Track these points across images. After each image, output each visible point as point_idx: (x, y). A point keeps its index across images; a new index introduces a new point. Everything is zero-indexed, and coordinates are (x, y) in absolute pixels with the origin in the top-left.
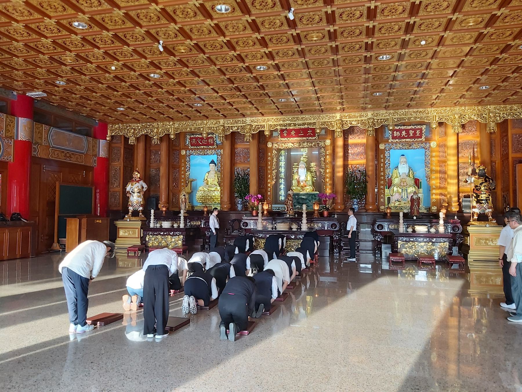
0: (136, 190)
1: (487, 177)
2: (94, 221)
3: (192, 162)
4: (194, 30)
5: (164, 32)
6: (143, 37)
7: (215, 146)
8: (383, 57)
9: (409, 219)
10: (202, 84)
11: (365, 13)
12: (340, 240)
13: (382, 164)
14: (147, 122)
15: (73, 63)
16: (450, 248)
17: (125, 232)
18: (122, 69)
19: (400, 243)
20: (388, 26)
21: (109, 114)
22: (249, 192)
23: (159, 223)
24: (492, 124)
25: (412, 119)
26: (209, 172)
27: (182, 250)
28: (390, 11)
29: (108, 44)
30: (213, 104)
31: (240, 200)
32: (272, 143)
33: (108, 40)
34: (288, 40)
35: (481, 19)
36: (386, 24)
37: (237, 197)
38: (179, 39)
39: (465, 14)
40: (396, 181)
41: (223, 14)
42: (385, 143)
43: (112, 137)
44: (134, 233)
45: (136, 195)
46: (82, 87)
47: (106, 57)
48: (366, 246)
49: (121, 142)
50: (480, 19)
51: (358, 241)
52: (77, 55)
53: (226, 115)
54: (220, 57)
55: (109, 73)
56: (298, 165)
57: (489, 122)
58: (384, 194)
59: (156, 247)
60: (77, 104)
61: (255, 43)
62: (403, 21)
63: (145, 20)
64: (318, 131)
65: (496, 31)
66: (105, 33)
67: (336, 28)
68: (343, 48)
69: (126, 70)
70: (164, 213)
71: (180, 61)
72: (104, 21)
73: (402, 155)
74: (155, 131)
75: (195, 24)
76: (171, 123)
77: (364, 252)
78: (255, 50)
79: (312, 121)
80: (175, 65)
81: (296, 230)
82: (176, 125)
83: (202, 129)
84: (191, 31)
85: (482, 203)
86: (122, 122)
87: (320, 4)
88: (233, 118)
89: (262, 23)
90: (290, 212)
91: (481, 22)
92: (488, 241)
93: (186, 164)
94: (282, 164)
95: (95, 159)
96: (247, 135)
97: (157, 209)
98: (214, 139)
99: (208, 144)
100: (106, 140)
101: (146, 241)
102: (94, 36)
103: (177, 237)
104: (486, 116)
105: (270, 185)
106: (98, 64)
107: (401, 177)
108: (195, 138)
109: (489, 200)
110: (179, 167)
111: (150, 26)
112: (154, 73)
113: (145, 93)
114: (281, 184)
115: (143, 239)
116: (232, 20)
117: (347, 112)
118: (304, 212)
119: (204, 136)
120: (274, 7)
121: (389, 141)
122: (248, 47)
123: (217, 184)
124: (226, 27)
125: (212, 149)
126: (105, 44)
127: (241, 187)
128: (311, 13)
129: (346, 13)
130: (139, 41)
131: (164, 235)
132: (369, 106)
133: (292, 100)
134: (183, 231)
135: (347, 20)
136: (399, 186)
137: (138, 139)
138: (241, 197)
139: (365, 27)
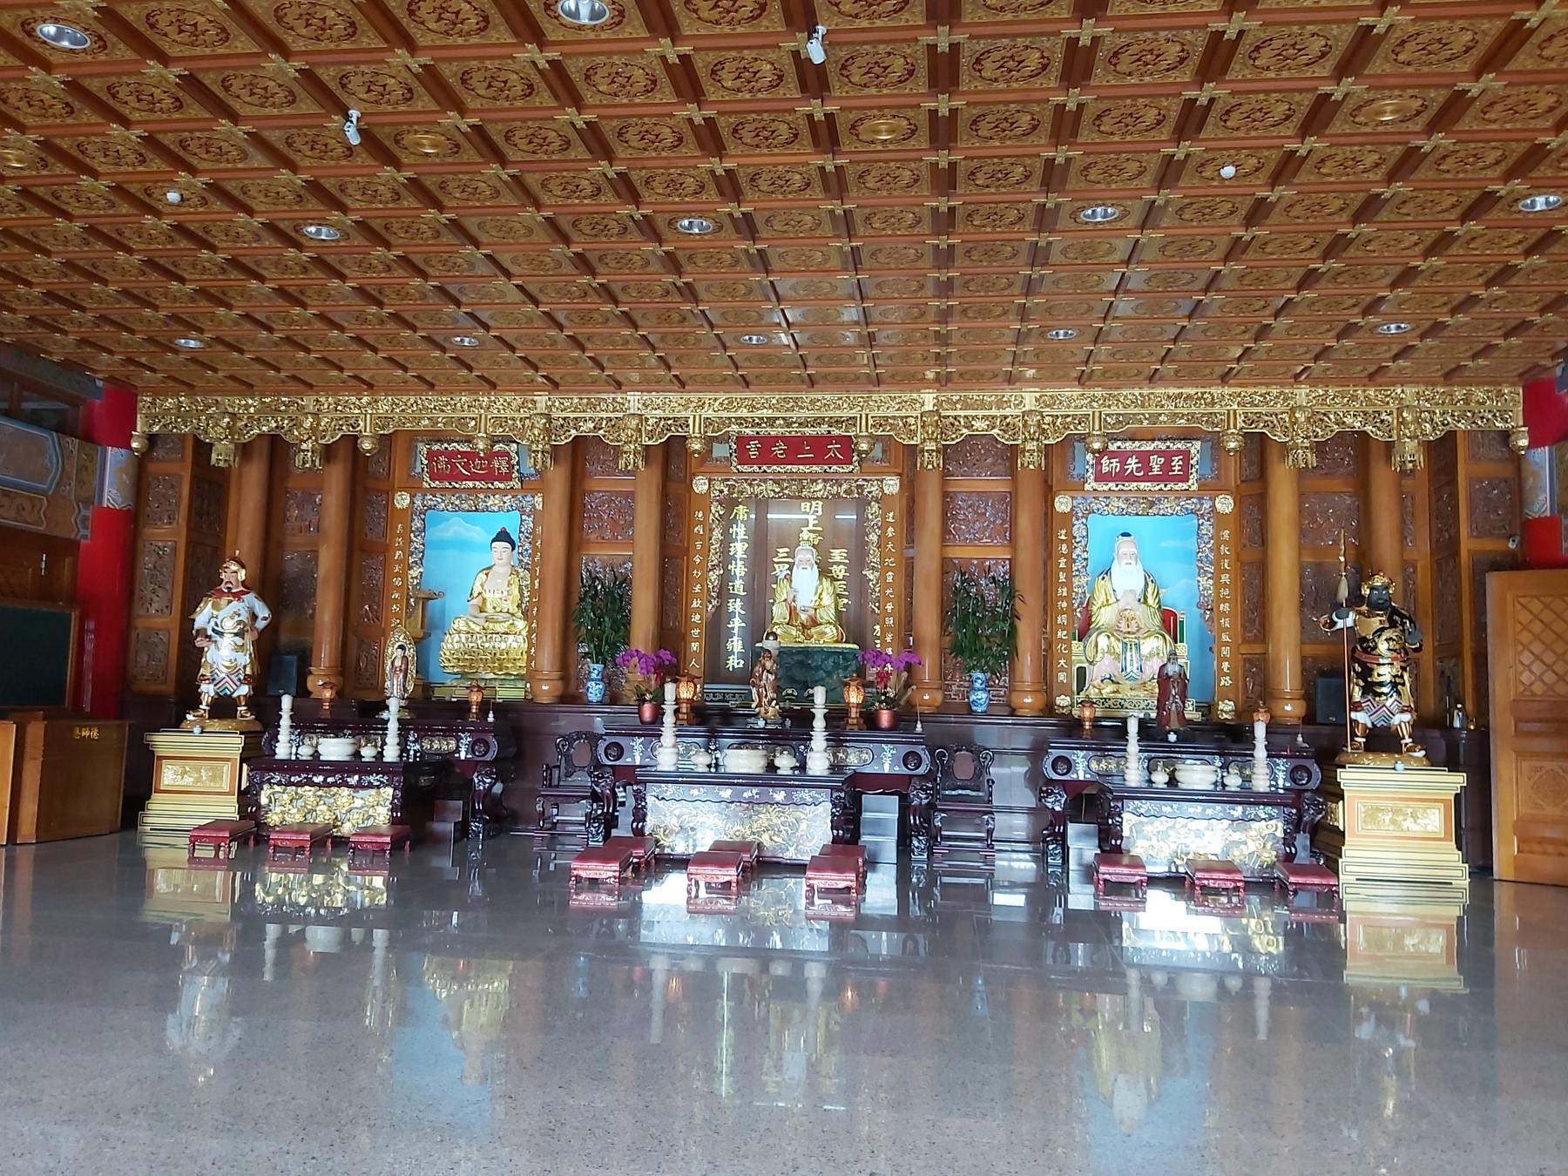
0: (229, 625)
1: (1395, 611)
2: (72, 731)
3: (433, 533)
4: (476, 80)
5: (367, 78)
6: (291, 93)
7: (516, 484)
8: (1094, 211)
9: (1154, 741)
10: (434, 299)
11: (1059, 56)
12: (932, 807)
13: (1063, 561)
14: (279, 393)
15: (26, 173)
16: (1288, 840)
17: (184, 773)
18: (205, 202)
19: (1128, 821)
20: (1123, 110)
21: (143, 360)
22: (626, 640)
23: (307, 741)
24: (1411, 446)
25: (1161, 419)
26: (490, 568)
27: (388, 840)
28: (1139, 60)
29: (161, 110)
30: (517, 340)
31: (596, 666)
32: (710, 481)
33: (163, 96)
34: (796, 136)
35: (1420, 102)
36: (989, 161)
37: (586, 655)
38: (419, 106)
39: (1375, 82)
40: (1104, 617)
41: (581, 28)
42: (1073, 494)
43: (152, 439)
44: (216, 777)
45: (227, 642)
46: (55, 260)
47: (149, 155)
48: (1012, 828)
49: (183, 459)
50: (1417, 104)
51: (992, 813)
52: (46, 145)
53: (557, 379)
54: (558, 181)
55: (158, 214)
56: (791, 555)
57: (1399, 438)
58: (1068, 657)
59: (295, 828)
60: (33, 320)
61: (680, 140)
62: (1174, 95)
63: (303, 31)
64: (864, 446)
65: (1457, 148)
66: (153, 67)
67: (958, 103)
68: (973, 173)
69: (218, 205)
70: (326, 706)
71: (415, 185)
72: (152, 26)
73: (1123, 535)
74: (307, 424)
75: (482, 59)
76: (365, 400)
77: (1006, 847)
78: (681, 163)
79: (846, 414)
80: (397, 197)
81: (790, 772)
82: (383, 407)
83: (473, 423)
84: (464, 82)
85: (1380, 695)
86: (190, 388)
87: (916, 15)
88: (580, 392)
89: (714, 72)
90: (767, 712)
91: (1418, 113)
92: (1401, 818)
93: (411, 541)
94: (739, 549)
95: (85, 512)
96: (626, 448)
97: (302, 693)
98: (510, 458)
99: (490, 476)
100: (130, 448)
101: (259, 806)
102: (114, 79)
103: (373, 792)
104: (1389, 418)
105: (698, 617)
106: (120, 178)
107: (1121, 605)
108: (445, 453)
109: (1403, 684)
110: (386, 550)
111: (320, 52)
112: (320, 222)
113: (281, 292)
114: (732, 614)
115: (247, 798)
116: (610, 54)
117: (956, 390)
118: (819, 712)
119: (481, 446)
120: (759, 15)
121: (1087, 487)
122: (655, 150)
123: (514, 609)
124: (587, 77)
125: (504, 492)
126: (152, 110)
127: (600, 624)
128: (881, 48)
129: (996, 56)
130: (273, 105)
131: (325, 785)
132: (1030, 373)
133: (785, 339)
134: (395, 774)
135: (996, 80)
136: (1113, 632)
137: (245, 451)
138: (598, 656)
139: (1050, 107)
